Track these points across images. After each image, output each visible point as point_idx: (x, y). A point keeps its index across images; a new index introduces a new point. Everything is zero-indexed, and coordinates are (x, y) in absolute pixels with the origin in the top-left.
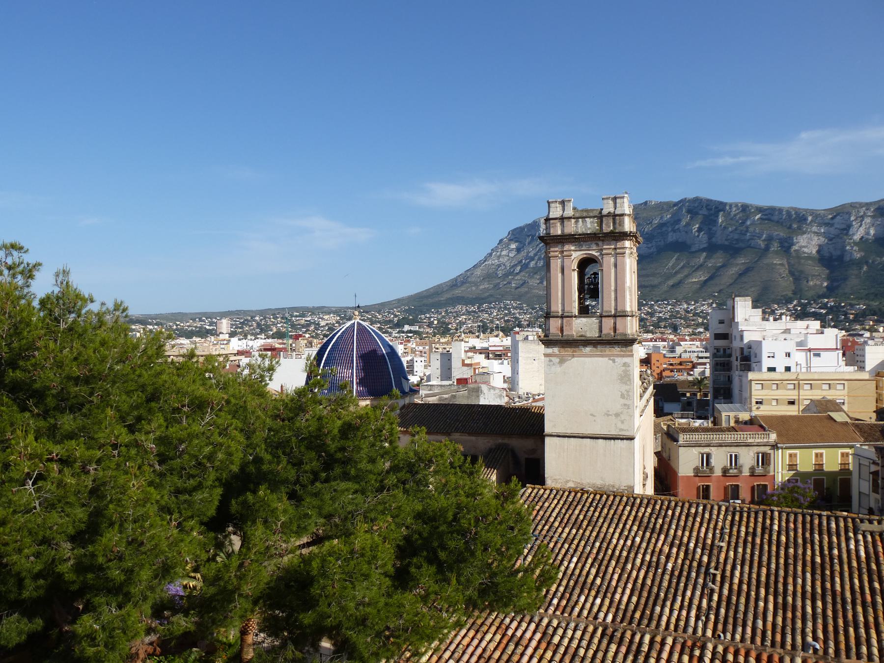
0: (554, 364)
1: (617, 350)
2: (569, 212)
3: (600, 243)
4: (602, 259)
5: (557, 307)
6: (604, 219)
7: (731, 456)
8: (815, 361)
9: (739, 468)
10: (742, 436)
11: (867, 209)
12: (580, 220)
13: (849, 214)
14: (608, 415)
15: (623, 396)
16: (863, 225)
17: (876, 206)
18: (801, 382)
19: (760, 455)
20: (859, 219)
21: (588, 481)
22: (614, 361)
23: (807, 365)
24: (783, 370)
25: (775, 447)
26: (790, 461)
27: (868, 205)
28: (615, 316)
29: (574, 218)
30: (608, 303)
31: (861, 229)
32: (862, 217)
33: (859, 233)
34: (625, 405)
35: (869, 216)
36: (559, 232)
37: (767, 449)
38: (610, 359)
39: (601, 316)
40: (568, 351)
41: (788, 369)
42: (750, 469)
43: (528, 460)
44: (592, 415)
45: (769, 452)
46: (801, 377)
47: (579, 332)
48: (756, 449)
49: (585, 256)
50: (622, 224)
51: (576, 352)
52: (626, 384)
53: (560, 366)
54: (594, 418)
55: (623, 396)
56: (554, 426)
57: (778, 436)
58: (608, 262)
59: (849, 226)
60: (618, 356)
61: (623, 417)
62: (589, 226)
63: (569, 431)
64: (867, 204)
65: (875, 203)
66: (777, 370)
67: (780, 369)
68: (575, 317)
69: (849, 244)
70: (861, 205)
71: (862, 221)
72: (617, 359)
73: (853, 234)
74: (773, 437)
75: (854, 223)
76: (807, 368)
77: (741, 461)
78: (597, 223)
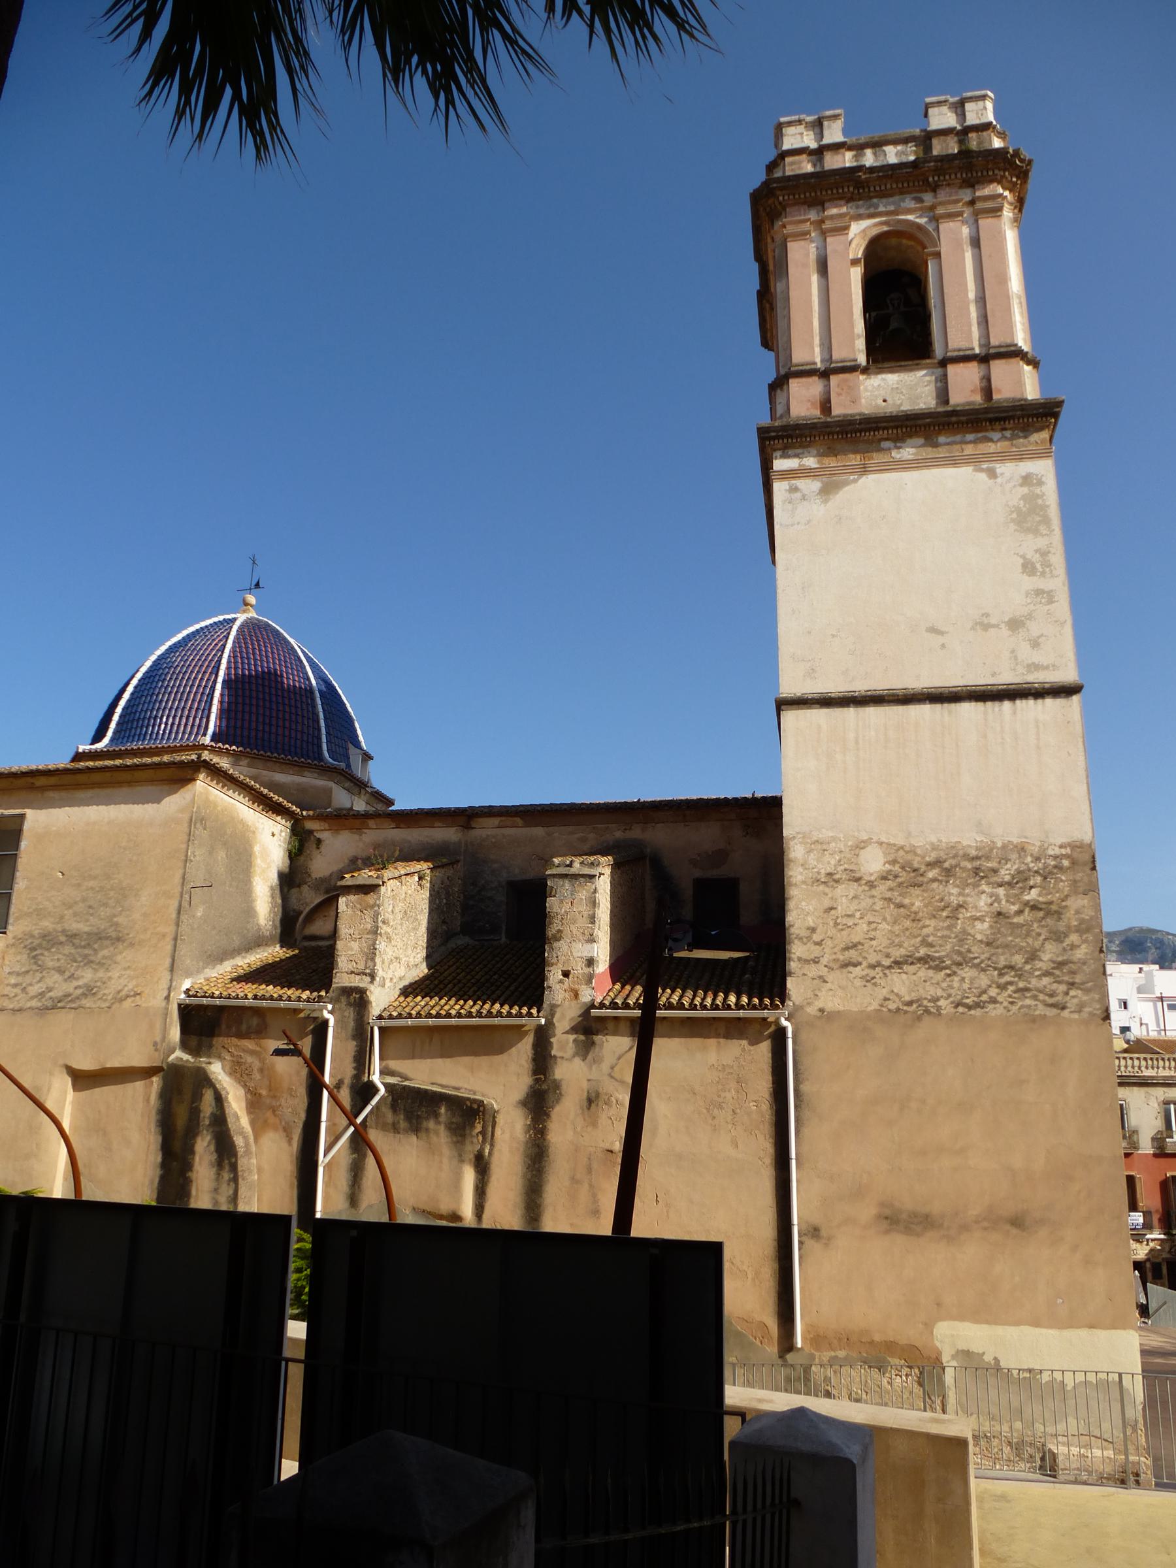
0: (804, 498)
2: (834, 133)
3: (928, 198)
4: (937, 229)
10: (1130, 1062)
14: (986, 627)
17: (1123, 938)
21: (933, 839)
22: (992, 474)
23: (1158, 1025)
29: (850, 148)
34: (1039, 592)
35: (1114, 951)
38: (982, 470)
39: (944, 363)
42: (1153, 1139)
43: (701, 885)
44: (933, 630)
48: (1161, 1093)
49: (885, 228)
52: (1036, 532)
53: (826, 501)
54: (941, 640)
56: (811, 673)
60: (1003, 457)
63: (860, 686)
68: (865, 371)
72: (1000, 468)
77: (1135, 1119)
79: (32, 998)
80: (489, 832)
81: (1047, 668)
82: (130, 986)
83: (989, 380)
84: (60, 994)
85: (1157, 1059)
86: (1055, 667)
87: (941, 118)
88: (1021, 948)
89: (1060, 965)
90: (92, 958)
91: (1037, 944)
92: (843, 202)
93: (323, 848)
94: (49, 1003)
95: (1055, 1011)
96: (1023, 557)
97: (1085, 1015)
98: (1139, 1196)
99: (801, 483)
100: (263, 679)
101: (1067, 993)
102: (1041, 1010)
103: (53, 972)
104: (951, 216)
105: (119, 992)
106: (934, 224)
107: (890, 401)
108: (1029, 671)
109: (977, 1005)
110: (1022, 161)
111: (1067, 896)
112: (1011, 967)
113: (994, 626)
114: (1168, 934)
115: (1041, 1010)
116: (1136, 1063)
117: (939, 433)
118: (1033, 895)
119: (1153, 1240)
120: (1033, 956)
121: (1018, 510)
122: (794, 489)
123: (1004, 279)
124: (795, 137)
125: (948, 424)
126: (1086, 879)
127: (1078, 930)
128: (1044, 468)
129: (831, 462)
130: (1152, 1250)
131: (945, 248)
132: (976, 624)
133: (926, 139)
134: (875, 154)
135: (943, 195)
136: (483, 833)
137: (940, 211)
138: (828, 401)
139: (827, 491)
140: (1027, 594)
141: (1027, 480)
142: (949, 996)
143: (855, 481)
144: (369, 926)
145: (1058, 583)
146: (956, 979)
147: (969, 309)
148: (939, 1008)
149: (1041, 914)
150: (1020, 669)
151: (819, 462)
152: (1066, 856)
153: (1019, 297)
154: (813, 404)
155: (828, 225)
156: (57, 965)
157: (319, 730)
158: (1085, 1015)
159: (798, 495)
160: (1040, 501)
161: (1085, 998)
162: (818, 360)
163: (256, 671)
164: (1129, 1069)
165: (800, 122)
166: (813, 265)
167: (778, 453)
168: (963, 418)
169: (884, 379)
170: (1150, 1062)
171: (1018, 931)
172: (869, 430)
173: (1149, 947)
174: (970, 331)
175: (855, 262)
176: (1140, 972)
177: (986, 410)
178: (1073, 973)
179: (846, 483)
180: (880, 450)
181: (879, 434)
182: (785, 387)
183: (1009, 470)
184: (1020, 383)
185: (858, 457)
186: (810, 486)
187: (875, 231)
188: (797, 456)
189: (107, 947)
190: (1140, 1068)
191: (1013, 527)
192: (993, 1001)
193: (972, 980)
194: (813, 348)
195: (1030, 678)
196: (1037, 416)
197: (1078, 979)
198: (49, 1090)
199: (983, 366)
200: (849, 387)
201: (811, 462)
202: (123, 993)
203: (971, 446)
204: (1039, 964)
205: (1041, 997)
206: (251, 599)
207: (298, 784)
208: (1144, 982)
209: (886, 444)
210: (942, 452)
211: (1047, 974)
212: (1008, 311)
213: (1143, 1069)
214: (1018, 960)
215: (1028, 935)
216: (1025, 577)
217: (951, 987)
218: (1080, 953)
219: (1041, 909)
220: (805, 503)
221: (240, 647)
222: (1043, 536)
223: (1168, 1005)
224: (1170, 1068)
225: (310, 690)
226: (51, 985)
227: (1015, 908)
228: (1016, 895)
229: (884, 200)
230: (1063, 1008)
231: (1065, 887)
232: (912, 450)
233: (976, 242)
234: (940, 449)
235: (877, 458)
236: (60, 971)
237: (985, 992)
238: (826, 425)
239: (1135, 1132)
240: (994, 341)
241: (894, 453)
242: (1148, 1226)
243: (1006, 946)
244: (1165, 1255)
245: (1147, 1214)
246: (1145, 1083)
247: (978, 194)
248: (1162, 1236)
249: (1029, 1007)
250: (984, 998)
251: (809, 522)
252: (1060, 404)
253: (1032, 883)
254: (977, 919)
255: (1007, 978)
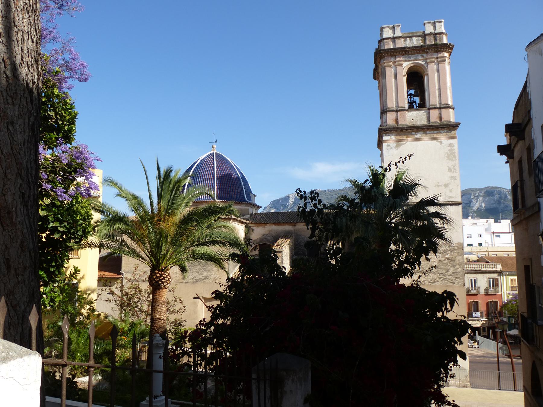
0: (391, 148)
1: (442, 135)
2: (398, 33)
3: (425, 55)
4: (427, 66)
5: (391, 104)
6: (427, 37)
7: (471, 280)
8: (497, 239)
9: (478, 289)
10: (478, 266)
11: (480, 192)
12: (408, 39)
13: (470, 195)
14: (439, 186)
15: (450, 170)
16: (478, 201)
17: (485, 191)
18: (490, 253)
19: (491, 280)
20: (476, 198)
22: (441, 143)
23: (492, 242)
24: (478, 245)
25: (501, 274)
26: (512, 284)
27: (480, 190)
28: (440, 108)
29: (403, 38)
30: (433, 99)
31: (477, 203)
32: (478, 197)
33: (476, 206)
34: (452, 177)
35: (482, 196)
36: (392, 47)
37: (495, 276)
38: (438, 142)
39: (429, 109)
40: (403, 137)
41: (480, 245)
42: (485, 290)
45: (497, 277)
46: (489, 250)
47: (411, 121)
48: (488, 276)
49: (413, 65)
50: (441, 39)
51: (409, 137)
52: (452, 160)
53: (397, 149)
55: (450, 170)
57: (502, 266)
58: (432, 68)
59: (471, 202)
60: (444, 138)
61: (451, 187)
62: (416, 42)
64: (480, 189)
65: (484, 189)
66: (473, 245)
67: (476, 244)
68: (407, 110)
69: (471, 212)
70: (477, 190)
71: (477, 199)
73: (473, 206)
74: (499, 267)
75: (473, 200)
76: (492, 244)
77: (479, 284)
78: (422, 40)
79: (190, 279)
80: (301, 227)
81: (453, 198)
82: (218, 276)
83: (441, 115)
84: (198, 278)
85: (487, 265)
86: (455, 197)
87: (429, 29)
88: (445, 269)
89: (454, 273)
90: (206, 269)
91: (449, 268)
92: (401, 56)
93: (254, 232)
94: (195, 281)
95: (452, 284)
96: (448, 167)
97: (459, 285)
98: (479, 307)
99: (390, 144)
100: (225, 177)
101: (455, 280)
102: (449, 284)
103: (195, 273)
104: (431, 62)
105: (215, 278)
106: (426, 64)
107: (414, 120)
108: (449, 198)
109: (434, 282)
110: (451, 46)
111: (456, 256)
112: (442, 273)
113: (440, 186)
114: (503, 189)
115: (449, 284)
116: (480, 266)
117: (427, 130)
118: (448, 256)
119: (483, 320)
120: (447, 271)
121: (447, 153)
122: (389, 146)
123: (445, 83)
124: (388, 33)
125: (430, 128)
126: (461, 252)
127: (459, 265)
128: (454, 141)
129: (399, 138)
130: (483, 324)
131: (430, 72)
132: (436, 185)
133: (424, 36)
134: (410, 40)
135: (429, 54)
136: (299, 227)
137: (429, 60)
138: (398, 119)
139: (398, 146)
140: (449, 177)
141: (450, 145)
142: (427, 280)
143: (405, 144)
144: (280, 261)
145: (457, 175)
146: (429, 276)
147: (436, 92)
148: (425, 283)
149: (450, 261)
150: (447, 198)
151: (395, 138)
152: (456, 246)
153: (450, 88)
154: (393, 120)
155: (397, 63)
156: (196, 271)
157: (243, 191)
158: (459, 285)
159: (390, 147)
160: (453, 151)
161: (459, 281)
162: (394, 106)
163: (223, 174)
164: (478, 268)
165: (388, 27)
166: (393, 76)
167: (384, 135)
168: (434, 127)
169: (413, 113)
170: (485, 266)
171: (444, 265)
172: (409, 129)
173: (496, 194)
174: (436, 99)
175: (404, 76)
176: (487, 222)
177: (440, 125)
178: (457, 275)
179: (403, 144)
180: (411, 135)
181: (411, 130)
182: (386, 114)
183: (446, 142)
184: (449, 116)
185: (406, 136)
186: (393, 145)
187: (410, 66)
188: (389, 136)
189: (210, 266)
190: (481, 268)
191: (446, 158)
192: (438, 281)
193: (433, 276)
194: (393, 103)
195: (449, 200)
196: (454, 127)
197: (458, 276)
198: (198, 302)
199: (440, 110)
200: (403, 116)
201: (393, 138)
202: (216, 278)
203: (436, 134)
204: (449, 273)
205: (449, 280)
206: (215, 146)
207: (240, 209)
208: (487, 227)
209: (413, 133)
210: (428, 136)
211: (451, 275)
212: (446, 93)
213: (482, 268)
214: (444, 272)
215: (446, 266)
216: (449, 172)
217: (428, 278)
218: (458, 270)
219: (450, 259)
220: (392, 150)
221: (218, 167)
222: (454, 161)
223: (496, 235)
224: (491, 268)
225: (239, 178)
226: (195, 276)
227: (444, 259)
228: (444, 256)
229: (413, 55)
230: (454, 283)
231: (456, 254)
232: (420, 135)
233: (438, 71)
234: (427, 135)
235: (411, 137)
236: (198, 272)
237: (436, 279)
238: (397, 128)
239: (479, 288)
240: (443, 103)
241: (415, 136)
242: (482, 316)
243: (441, 268)
244: (487, 325)
245: (482, 313)
246: (483, 273)
247: (439, 55)
248: (486, 319)
249: (446, 283)
250: (436, 281)
251: (393, 155)
252: (459, 124)
253: (448, 253)
254: (434, 262)
255: (441, 276)
